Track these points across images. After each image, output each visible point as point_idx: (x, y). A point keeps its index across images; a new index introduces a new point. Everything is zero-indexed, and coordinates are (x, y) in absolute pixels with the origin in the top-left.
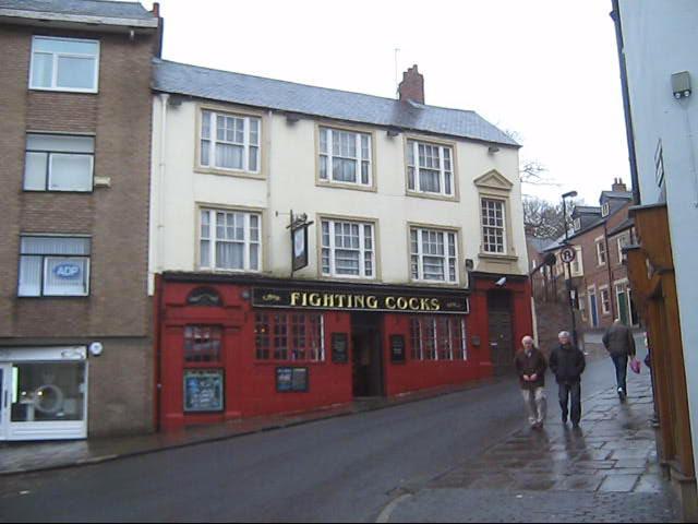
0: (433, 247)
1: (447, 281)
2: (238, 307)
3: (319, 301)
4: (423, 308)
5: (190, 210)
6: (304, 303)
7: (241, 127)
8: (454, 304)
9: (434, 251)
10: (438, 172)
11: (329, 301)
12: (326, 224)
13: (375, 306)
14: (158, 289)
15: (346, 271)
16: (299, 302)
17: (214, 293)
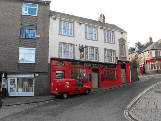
1: (112, 62)
2: (68, 66)
14: (51, 62)
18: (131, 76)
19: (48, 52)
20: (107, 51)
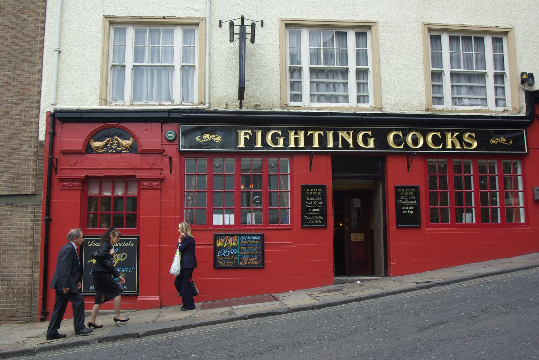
2: (161, 152)
3: (281, 141)
4: (449, 146)
6: (259, 144)
8: (502, 140)
9: (469, 64)
11: (297, 140)
13: (371, 145)
14: (52, 134)
15: (329, 99)
16: (250, 142)
19: (40, 79)
20: (445, 39)
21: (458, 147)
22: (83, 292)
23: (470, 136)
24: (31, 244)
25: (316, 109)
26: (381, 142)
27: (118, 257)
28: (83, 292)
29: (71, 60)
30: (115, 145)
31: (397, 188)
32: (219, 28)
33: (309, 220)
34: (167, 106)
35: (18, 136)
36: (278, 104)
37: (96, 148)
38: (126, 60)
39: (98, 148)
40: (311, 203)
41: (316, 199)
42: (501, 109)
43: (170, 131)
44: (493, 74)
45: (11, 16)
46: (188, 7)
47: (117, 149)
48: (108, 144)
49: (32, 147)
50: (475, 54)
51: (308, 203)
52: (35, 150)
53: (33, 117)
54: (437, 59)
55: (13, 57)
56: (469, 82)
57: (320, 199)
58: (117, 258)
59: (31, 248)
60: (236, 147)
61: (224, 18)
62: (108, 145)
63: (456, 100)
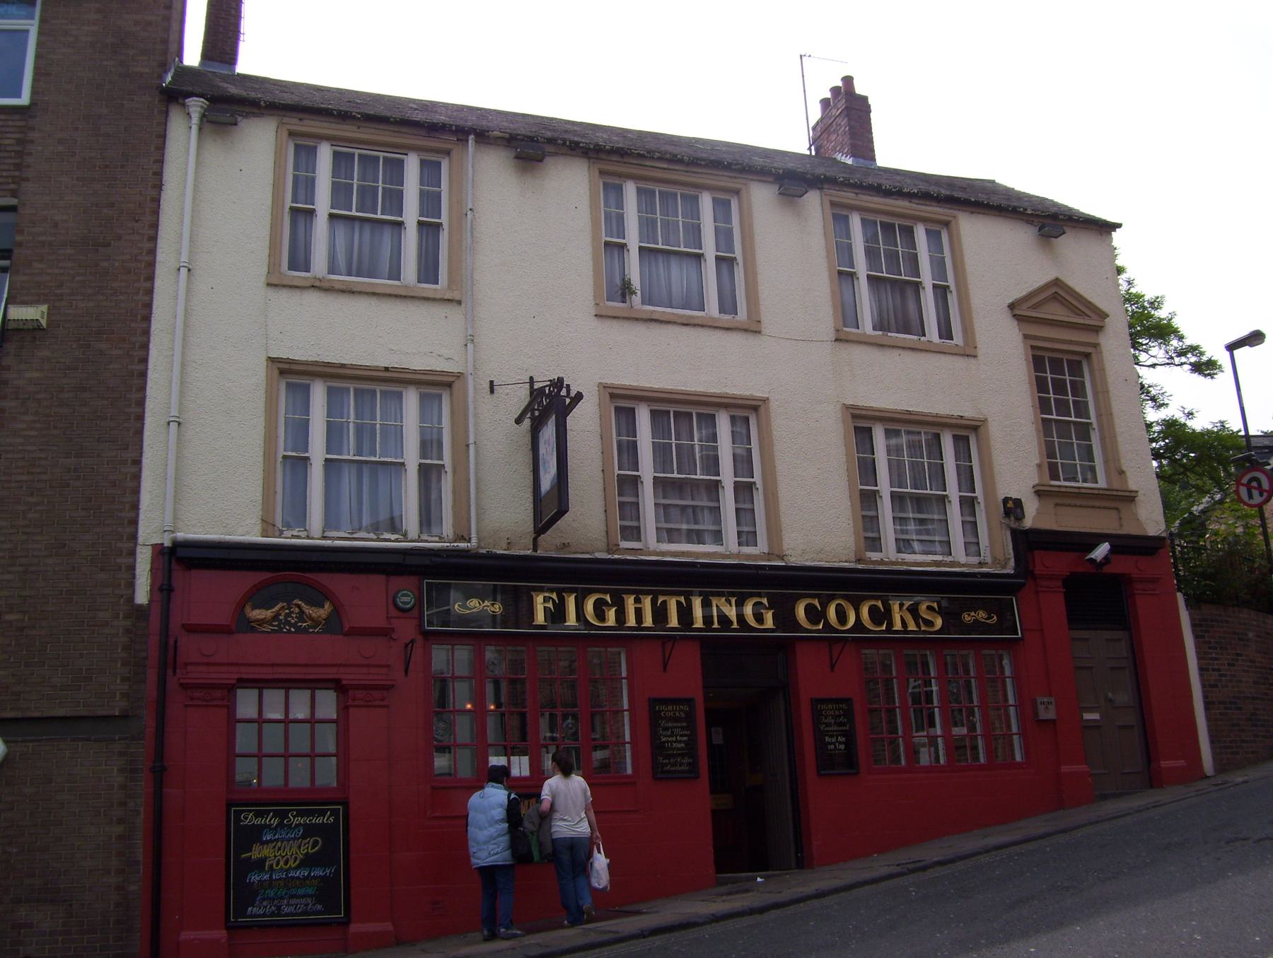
0: (686, 455)
1: (960, 558)
2: (385, 633)
3: (611, 615)
5: (255, 376)
6: (572, 620)
7: (694, 212)
10: (917, 286)
11: (639, 613)
12: (626, 416)
13: (769, 622)
14: (163, 588)
16: (557, 614)
17: (319, 596)
18: (1208, 705)
21: (912, 626)
22: (232, 920)
23: (929, 608)
24: (121, 821)
25: (671, 556)
26: (785, 618)
27: (303, 844)
28: (232, 920)
29: (202, 442)
30: (295, 616)
31: (816, 702)
32: (488, 395)
33: (666, 765)
34: (393, 541)
35: (88, 593)
36: (602, 545)
37: (258, 623)
38: (310, 448)
39: (262, 622)
40: (669, 733)
41: (679, 725)
42: (974, 560)
43: (404, 592)
44: (733, 485)
45: (72, 345)
46: (431, 352)
47: (300, 624)
48: (280, 615)
49: (121, 616)
50: (928, 462)
51: (664, 733)
52: (128, 623)
53: (121, 555)
54: (867, 470)
55: (75, 428)
56: (919, 512)
57: (684, 724)
58: (302, 848)
59: (118, 829)
60: (531, 626)
61: (497, 376)
62: (280, 617)
63: (903, 545)
